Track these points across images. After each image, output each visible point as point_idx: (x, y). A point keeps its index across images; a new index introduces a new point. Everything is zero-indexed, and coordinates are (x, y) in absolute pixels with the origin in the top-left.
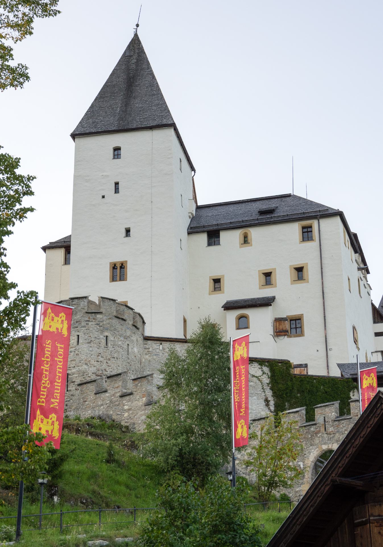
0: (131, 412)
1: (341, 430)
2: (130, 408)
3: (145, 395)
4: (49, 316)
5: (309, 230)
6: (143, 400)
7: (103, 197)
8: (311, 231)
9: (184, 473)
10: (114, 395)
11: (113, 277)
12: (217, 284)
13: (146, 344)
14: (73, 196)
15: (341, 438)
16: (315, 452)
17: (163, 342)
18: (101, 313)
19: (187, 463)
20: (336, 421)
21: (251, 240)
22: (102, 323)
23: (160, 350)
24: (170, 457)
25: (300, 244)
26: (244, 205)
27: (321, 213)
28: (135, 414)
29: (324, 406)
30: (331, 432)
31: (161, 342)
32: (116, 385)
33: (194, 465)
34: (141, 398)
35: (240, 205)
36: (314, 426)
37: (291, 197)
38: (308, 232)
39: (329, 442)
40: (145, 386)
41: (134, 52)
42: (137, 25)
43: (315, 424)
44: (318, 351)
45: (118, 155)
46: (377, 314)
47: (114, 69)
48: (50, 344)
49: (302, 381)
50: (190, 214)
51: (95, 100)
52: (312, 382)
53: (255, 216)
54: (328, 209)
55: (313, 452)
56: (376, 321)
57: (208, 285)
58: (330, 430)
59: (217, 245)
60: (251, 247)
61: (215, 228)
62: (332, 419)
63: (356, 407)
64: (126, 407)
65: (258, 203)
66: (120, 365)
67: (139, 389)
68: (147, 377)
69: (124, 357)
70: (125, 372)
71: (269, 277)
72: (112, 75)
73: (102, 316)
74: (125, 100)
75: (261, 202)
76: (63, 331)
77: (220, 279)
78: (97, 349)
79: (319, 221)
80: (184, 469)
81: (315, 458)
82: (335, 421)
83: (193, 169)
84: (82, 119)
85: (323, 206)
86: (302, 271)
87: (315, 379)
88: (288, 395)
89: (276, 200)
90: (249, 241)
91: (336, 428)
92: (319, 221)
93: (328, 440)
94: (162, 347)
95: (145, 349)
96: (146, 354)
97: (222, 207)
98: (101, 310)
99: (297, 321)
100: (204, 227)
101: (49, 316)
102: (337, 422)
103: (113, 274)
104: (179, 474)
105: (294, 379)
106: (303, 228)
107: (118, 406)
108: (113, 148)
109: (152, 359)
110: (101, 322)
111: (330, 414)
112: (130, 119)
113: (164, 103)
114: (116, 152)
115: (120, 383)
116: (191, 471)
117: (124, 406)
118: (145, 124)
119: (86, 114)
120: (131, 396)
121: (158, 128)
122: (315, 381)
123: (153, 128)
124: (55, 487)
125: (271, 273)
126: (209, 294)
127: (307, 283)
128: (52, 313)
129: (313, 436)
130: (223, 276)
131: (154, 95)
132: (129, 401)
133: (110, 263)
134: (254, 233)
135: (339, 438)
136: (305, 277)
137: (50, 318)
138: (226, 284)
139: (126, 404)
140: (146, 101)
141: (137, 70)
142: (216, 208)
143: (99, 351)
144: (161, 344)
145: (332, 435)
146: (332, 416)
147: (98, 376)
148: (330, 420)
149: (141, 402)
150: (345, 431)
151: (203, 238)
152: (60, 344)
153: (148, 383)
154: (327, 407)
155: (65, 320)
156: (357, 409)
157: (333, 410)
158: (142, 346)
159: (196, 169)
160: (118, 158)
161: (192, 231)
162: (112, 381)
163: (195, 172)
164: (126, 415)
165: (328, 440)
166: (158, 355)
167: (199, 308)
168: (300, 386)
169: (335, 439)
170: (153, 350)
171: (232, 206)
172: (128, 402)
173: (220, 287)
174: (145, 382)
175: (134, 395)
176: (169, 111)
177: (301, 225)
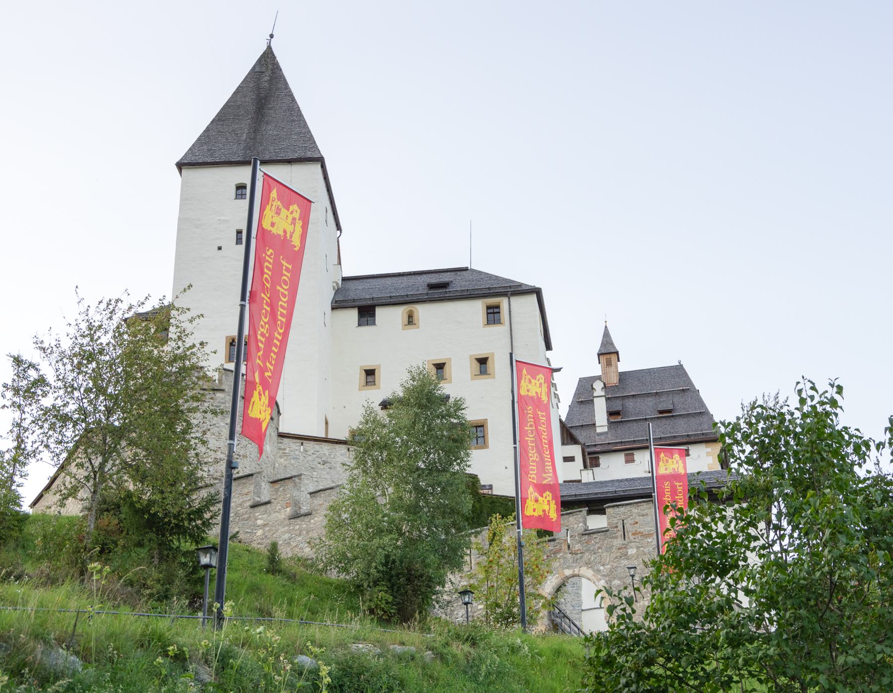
0: (267, 529)
1: (592, 548)
2: (266, 523)
3: (290, 503)
4: (272, 205)
5: (496, 310)
6: (286, 511)
7: (220, 248)
8: (499, 313)
9: (393, 590)
10: (241, 505)
11: (230, 357)
12: (369, 377)
13: (281, 443)
14: (177, 245)
15: (592, 559)
16: (553, 580)
17: (305, 442)
18: (222, 390)
19: (398, 575)
20: (585, 534)
21: (418, 320)
22: (224, 405)
23: (300, 452)
24: (374, 564)
25: (483, 327)
26: (405, 278)
27: (512, 290)
28: (274, 531)
29: (566, 514)
30: (578, 550)
31: (302, 441)
32: (246, 491)
33: (408, 580)
34: (284, 508)
35: (401, 278)
36: (552, 543)
37: (468, 272)
38: (494, 313)
39: (574, 565)
40: (290, 491)
41: (267, 68)
42: (272, 36)
43: (554, 540)
44: (506, 468)
45: (242, 195)
46: (567, 434)
47: (239, 87)
48: (272, 257)
49: (493, 502)
50: (335, 284)
51: (212, 122)
52: (507, 505)
53: (423, 290)
54: (521, 285)
55: (550, 580)
56: (566, 442)
57: (358, 377)
58: (576, 549)
59: (371, 325)
60: (417, 330)
61: (369, 303)
62: (579, 532)
63: (615, 515)
64: (259, 522)
65: (424, 276)
66: (247, 467)
67: (280, 495)
68: (293, 479)
69: (252, 456)
70: (259, 473)
71: (442, 370)
72: (236, 93)
73: (223, 396)
74: (253, 125)
75: (429, 276)
76: (293, 239)
77: (374, 370)
78: (215, 441)
79: (509, 299)
80: (393, 585)
81: (553, 588)
82: (583, 535)
83: (339, 227)
84: (193, 145)
85: (514, 281)
86: (486, 364)
87: (510, 501)
88: (475, 520)
89: (449, 273)
90: (415, 321)
91: (585, 544)
92: (509, 299)
93: (573, 562)
94: (304, 449)
95: (280, 449)
96: (281, 457)
97: (375, 280)
98: (223, 387)
99: (479, 429)
100: (354, 300)
101: (272, 205)
102: (586, 537)
103: (230, 352)
104: (386, 592)
105: (483, 499)
106: (488, 308)
107: (247, 520)
108: (236, 185)
109: (288, 464)
110: (223, 403)
111: (576, 525)
112: (261, 148)
113: (308, 132)
114: (239, 192)
115: (252, 488)
116: (403, 588)
117: (257, 520)
118: (282, 156)
119: (199, 139)
120: (268, 506)
121: (299, 162)
122: (510, 503)
123: (294, 162)
124: (200, 598)
125: (444, 364)
126: (360, 390)
127: (492, 379)
128: (278, 200)
129: (551, 556)
130: (379, 366)
131: (293, 121)
132: (265, 512)
133: (227, 337)
134: (423, 311)
135: (590, 559)
136: (490, 370)
137: (273, 208)
138: (382, 376)
139: (260, 517)
140: (284, 128)
141: (270, 89)
142: (368, 280)
143: (218, 444)
144: (302, 444)
145: (579, 555)
146: (579, 529)
147: (216, 479)
148: (576, 534)
149: (284, 513)
150: (598, 549)
151: (354, 314)
152: (286, 262)
153: (294, 487)
154: (571, 515)
155: (299, 220)
156: (615, 517)
157: (581, 520)
158: (275, 444)
159: (342, 228)
160: (242, 198)
161: (338, 305)
162: (239, 485)
163: (341, 232)
164: (260, 532)
165: (573, 562)
166: (297, 458)
167: (345, 407)
168: (491, 509)
169: (583, 560)
170: (291, 451)
171: (390, 279)
172: (263, 514)
173: (374, 382)
174: (290, 484)
175: (272, 504)
176: (315, 142)
177: (486, 303)
